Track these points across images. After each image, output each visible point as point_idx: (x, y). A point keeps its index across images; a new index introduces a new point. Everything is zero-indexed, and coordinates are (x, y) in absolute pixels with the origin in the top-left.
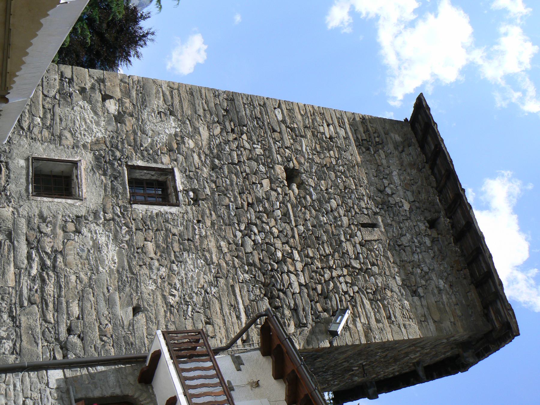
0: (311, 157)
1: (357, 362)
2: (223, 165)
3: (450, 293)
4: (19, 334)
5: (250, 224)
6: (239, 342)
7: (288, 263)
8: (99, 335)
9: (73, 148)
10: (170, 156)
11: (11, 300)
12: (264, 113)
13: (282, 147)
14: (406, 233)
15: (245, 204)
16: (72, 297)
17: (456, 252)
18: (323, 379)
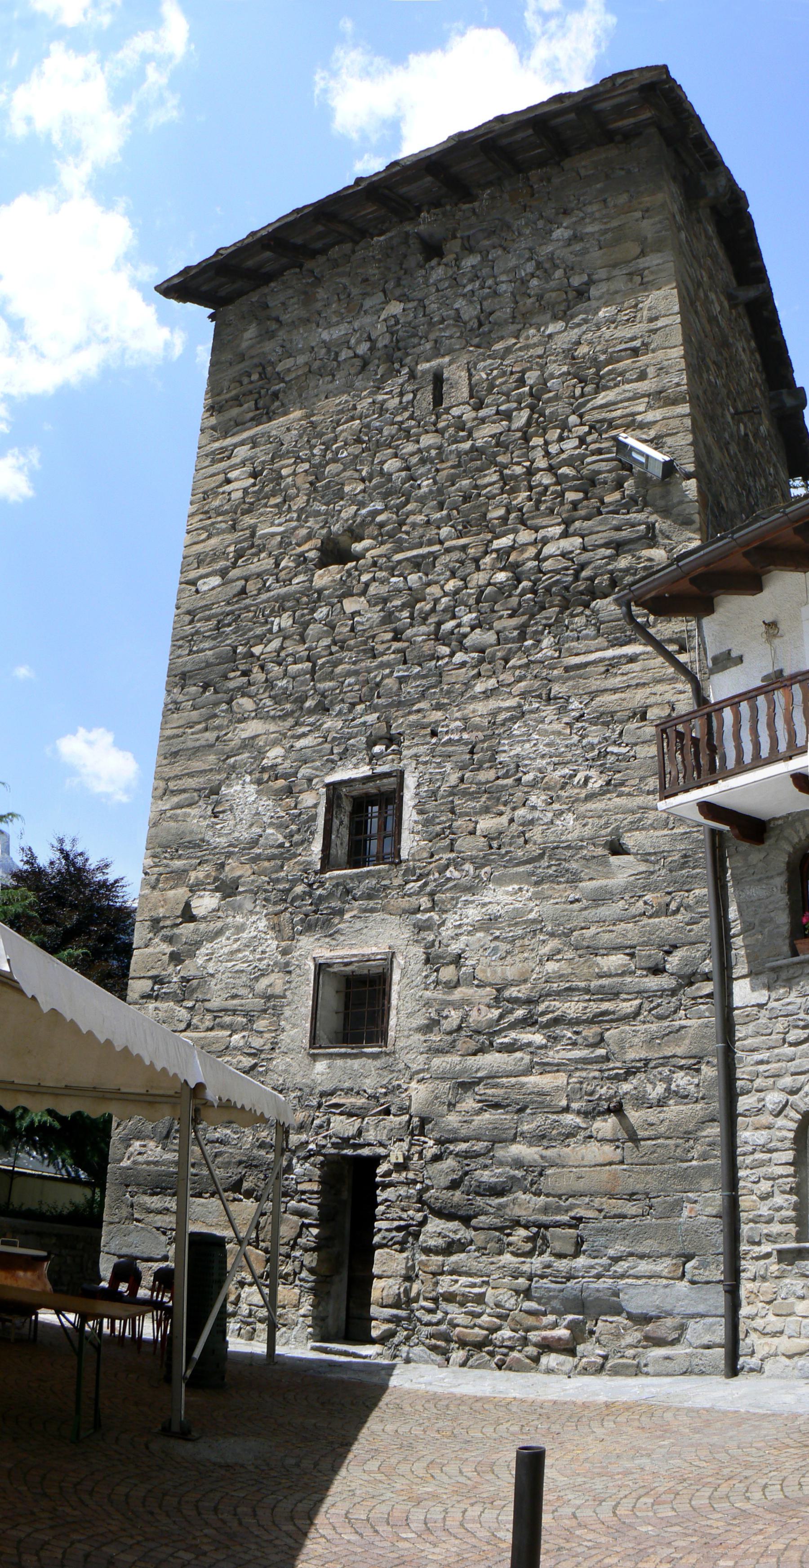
0: (295, 515)
1: (730, 426)
2: (316, 690)
3: (581, 215)
4: (661, 1061)
5: (437, 637)
6: (683, 658)
7: (520, 559)
8: (667, 916)
9: (290, 972)
10: (300, 792)
11: (595, 1078)
12: (207, 613)
13: (277, 574)
14: (452, 309)
15: (396, 645)
16: (589, 967)
17: (492, 198)
18: (763, 496)
